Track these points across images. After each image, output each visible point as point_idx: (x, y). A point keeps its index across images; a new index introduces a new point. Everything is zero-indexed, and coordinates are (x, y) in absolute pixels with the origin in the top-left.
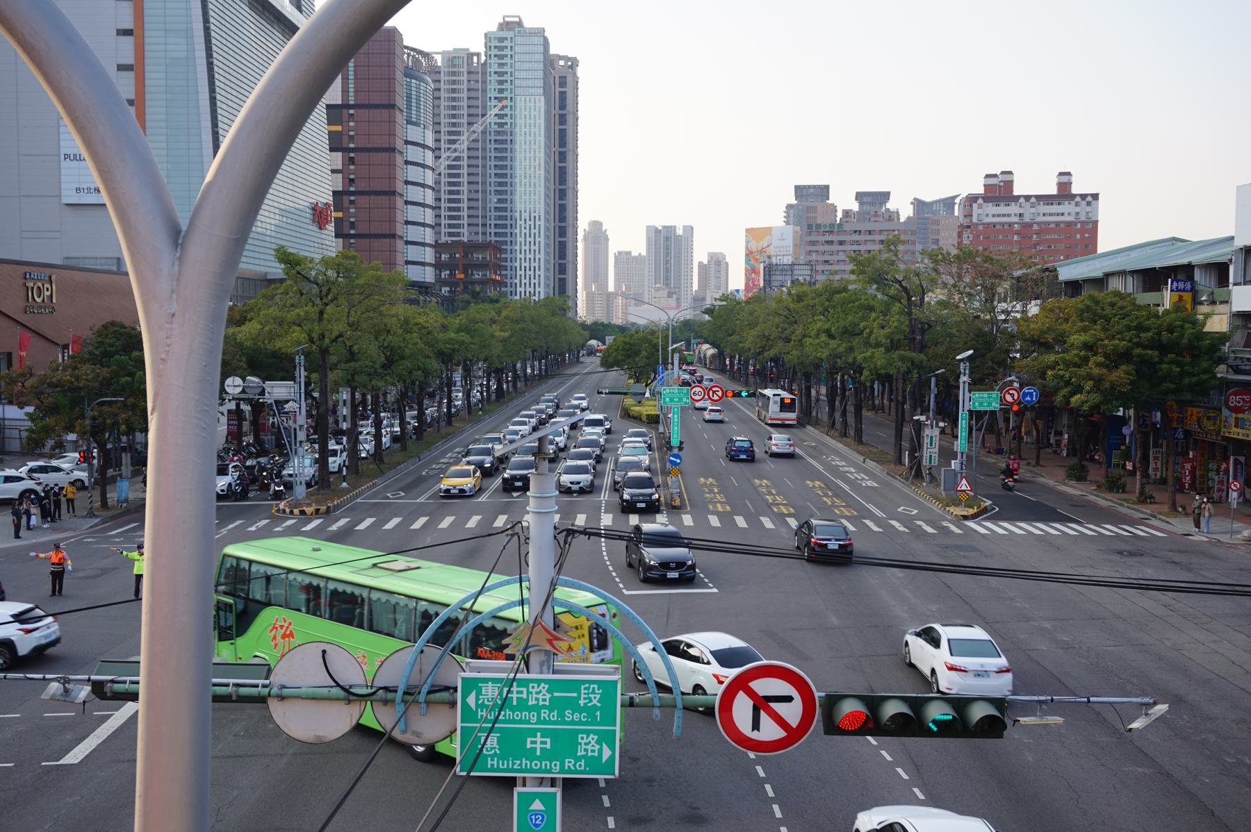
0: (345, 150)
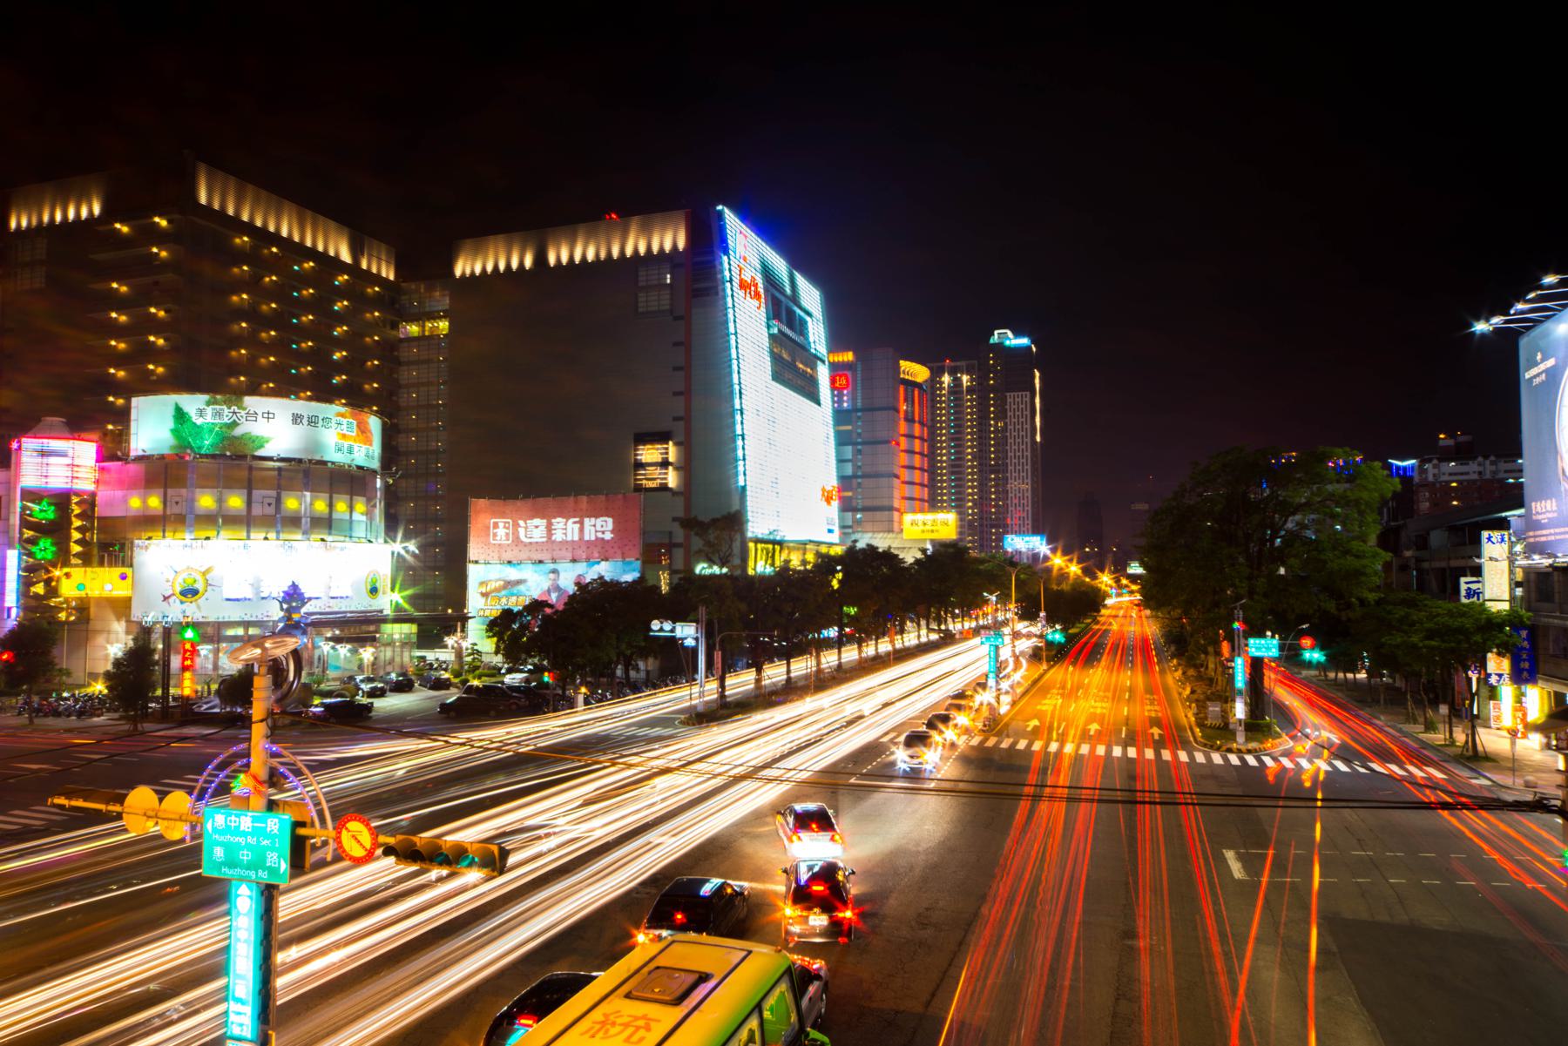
0: (854, 444)
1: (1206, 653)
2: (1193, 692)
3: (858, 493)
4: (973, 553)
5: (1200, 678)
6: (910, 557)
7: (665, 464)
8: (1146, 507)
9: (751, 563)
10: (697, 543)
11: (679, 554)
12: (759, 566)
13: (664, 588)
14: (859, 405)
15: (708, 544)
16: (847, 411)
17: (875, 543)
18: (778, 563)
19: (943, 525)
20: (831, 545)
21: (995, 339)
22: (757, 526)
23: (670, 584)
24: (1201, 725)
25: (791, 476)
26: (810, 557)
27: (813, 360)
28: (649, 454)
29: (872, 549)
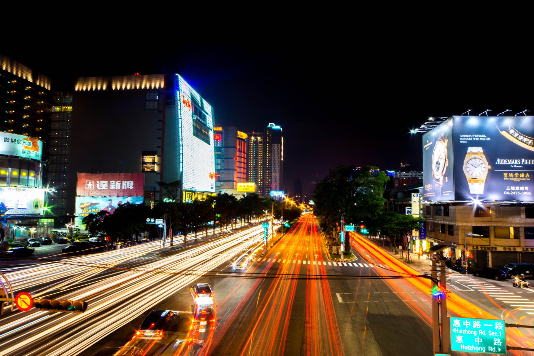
0: (221, 159)
1: (333, 230)
2: (328, 243)
3: (223, 175)
4: (260, 197)
5: (330, 238)
6: (239, 198)
7: (154, 163)
8: (315, 183)
9: (184, 199)
10: (164, 191)
11: (158, 195)
12: (187, 199)
13: (152, 207)
14: (223, 145)
15: (168, 191)
16: (219, 147)
17: (227, 192)
18: (193, 199)
19: (250, 187)
20: (212, 193)
21: (269, 126)
22: (186, 185)
23: (154, 205)
24: (331, 253)
25: (199, 168)
26: (205, 197)
27: (208, 129)
28: (148, 159)
29: (226, 195)
